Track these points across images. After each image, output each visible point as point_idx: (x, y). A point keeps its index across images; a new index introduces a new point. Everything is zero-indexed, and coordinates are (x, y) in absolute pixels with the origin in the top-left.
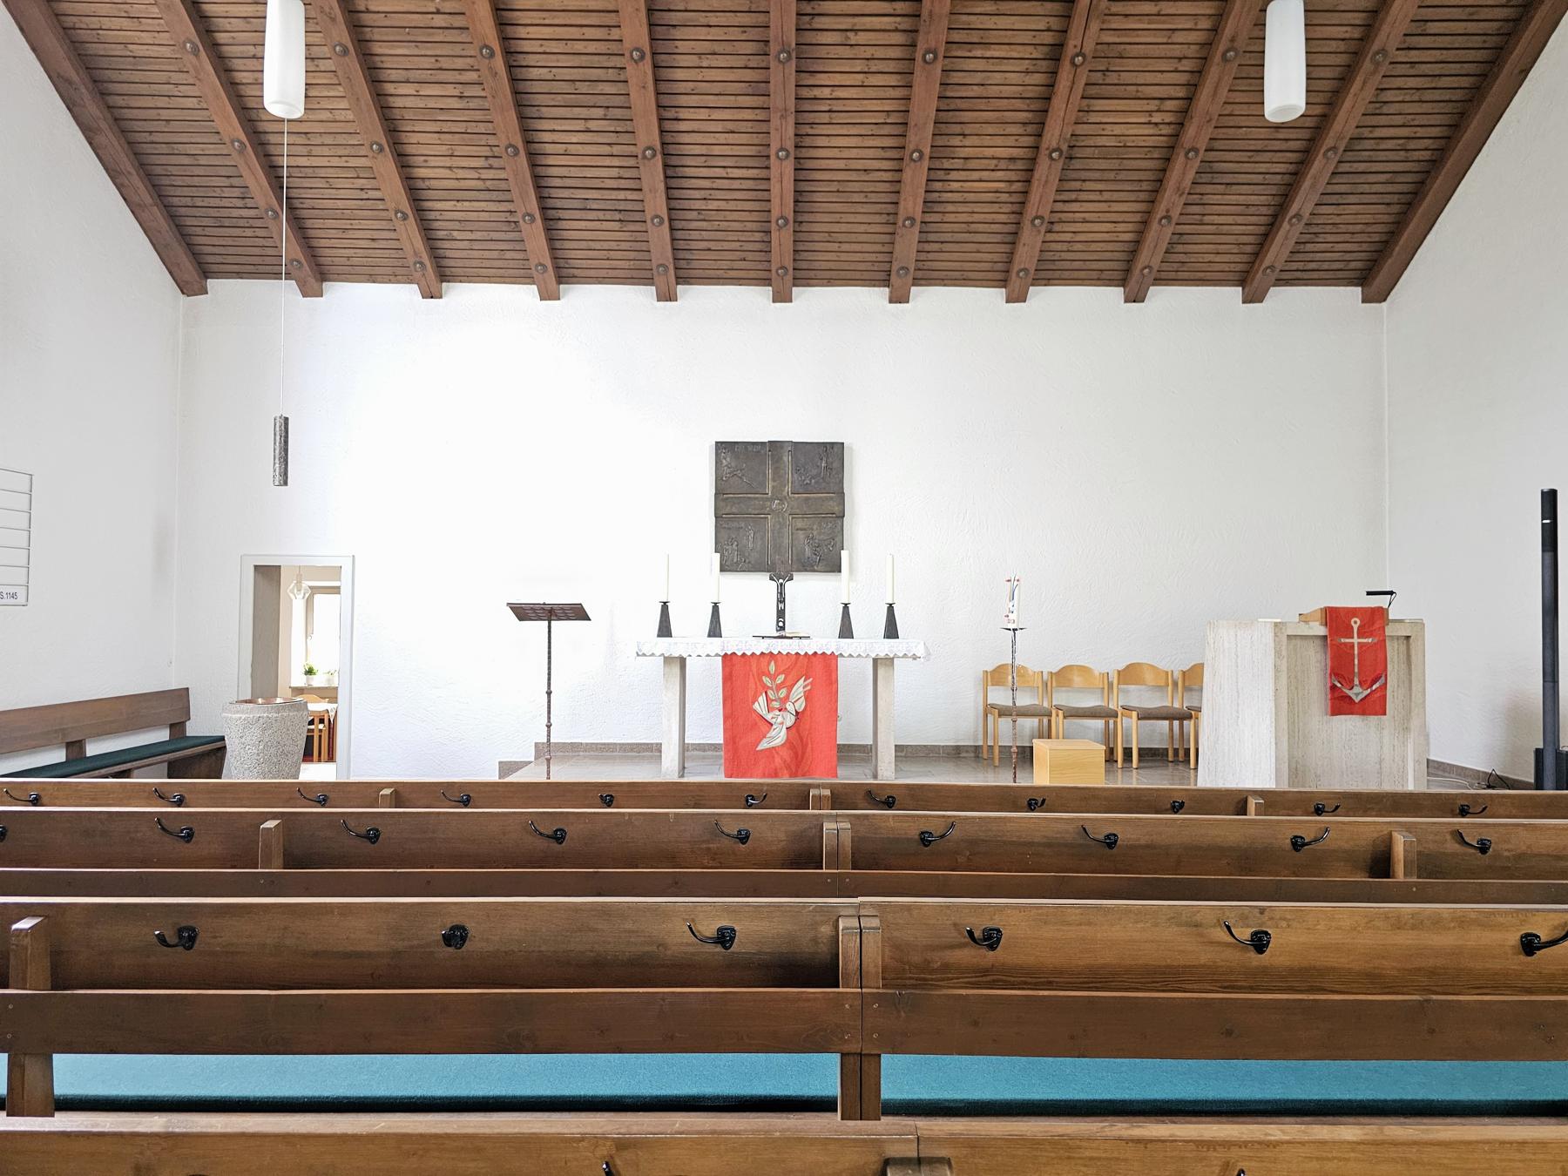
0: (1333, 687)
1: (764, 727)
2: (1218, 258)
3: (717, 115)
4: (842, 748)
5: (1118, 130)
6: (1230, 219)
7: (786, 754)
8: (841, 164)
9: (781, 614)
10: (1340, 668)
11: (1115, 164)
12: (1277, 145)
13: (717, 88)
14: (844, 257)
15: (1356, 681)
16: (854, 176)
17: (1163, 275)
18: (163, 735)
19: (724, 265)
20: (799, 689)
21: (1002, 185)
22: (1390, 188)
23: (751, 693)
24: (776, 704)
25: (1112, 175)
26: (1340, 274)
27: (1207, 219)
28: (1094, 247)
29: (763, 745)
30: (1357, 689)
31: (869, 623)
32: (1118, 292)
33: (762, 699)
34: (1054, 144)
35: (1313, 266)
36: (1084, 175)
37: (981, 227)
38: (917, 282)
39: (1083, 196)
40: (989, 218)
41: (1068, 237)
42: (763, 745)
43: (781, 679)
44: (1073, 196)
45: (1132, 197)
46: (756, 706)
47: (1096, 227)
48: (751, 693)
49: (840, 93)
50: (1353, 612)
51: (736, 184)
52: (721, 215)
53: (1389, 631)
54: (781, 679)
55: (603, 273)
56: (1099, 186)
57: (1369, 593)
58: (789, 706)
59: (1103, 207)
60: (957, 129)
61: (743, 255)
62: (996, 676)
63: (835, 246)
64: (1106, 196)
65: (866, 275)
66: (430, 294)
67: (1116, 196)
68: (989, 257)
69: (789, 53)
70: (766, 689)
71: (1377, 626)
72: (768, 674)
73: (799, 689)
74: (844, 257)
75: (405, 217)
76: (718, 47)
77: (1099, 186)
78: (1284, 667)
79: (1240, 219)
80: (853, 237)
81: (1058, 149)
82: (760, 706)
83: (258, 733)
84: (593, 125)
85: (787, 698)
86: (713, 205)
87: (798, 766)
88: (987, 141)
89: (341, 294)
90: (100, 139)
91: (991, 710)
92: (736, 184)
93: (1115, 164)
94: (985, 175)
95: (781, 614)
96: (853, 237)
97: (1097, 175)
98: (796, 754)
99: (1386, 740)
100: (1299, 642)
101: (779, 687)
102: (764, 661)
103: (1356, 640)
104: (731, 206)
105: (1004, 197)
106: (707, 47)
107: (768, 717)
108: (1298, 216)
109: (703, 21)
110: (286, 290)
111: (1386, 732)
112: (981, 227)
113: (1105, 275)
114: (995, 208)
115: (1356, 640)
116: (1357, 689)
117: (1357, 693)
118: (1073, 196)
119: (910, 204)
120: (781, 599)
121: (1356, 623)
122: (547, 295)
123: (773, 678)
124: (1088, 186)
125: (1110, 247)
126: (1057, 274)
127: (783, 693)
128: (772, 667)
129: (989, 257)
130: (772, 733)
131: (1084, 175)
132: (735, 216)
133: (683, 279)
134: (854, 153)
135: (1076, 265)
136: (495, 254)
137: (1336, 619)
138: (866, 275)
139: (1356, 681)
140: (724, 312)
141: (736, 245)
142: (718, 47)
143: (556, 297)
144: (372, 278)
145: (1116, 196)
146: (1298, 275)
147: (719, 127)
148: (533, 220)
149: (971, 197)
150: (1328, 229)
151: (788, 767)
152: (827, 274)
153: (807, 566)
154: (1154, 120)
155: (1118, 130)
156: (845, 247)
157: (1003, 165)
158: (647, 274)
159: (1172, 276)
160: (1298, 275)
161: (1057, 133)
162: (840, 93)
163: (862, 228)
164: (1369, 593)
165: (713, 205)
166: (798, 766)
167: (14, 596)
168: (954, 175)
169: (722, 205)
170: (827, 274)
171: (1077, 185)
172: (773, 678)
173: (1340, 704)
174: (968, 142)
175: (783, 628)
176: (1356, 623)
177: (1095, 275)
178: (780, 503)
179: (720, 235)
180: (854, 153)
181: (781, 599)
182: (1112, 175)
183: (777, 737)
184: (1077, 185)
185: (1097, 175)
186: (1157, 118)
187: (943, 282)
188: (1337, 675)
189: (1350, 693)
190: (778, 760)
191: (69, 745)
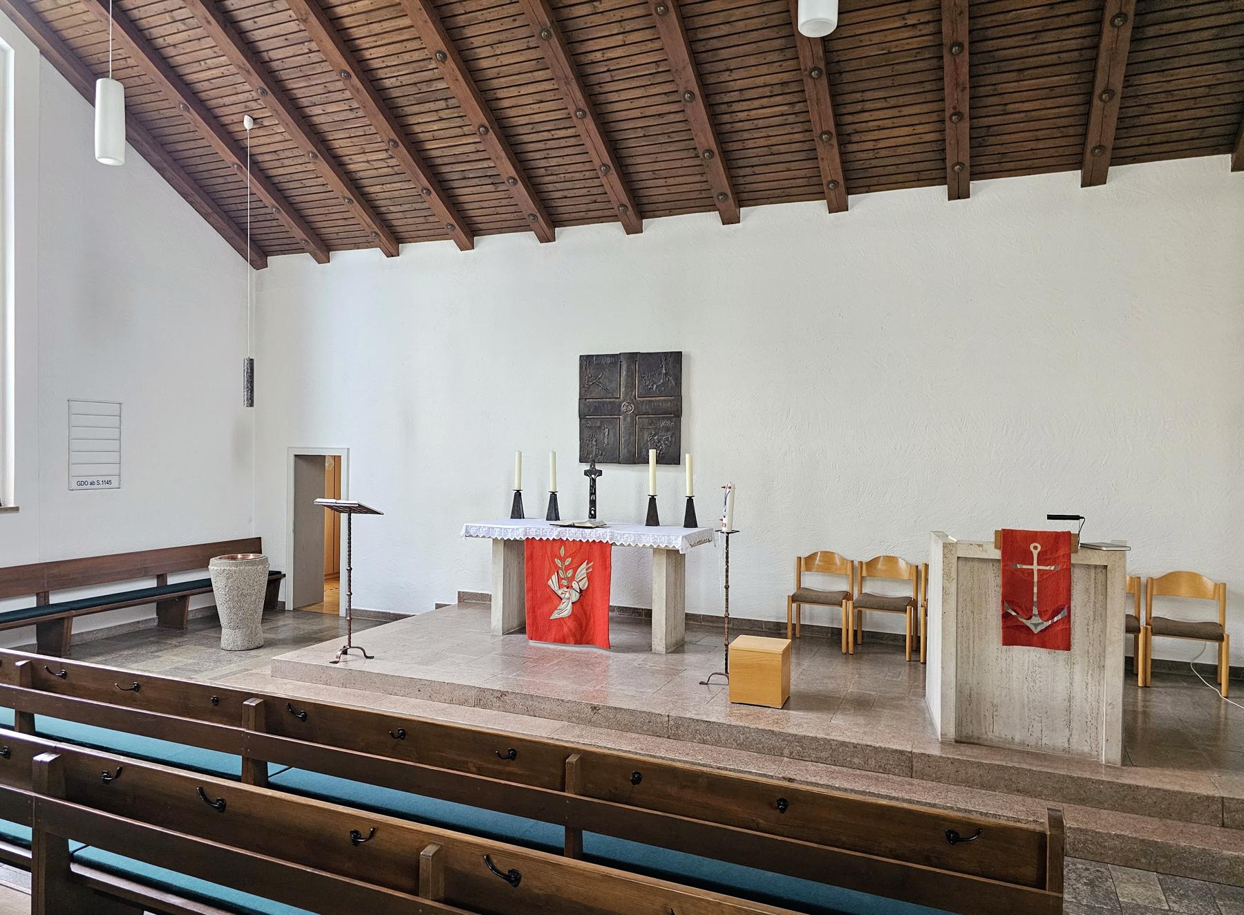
0: (1006, 616)
1: (556, 601)
2: (1041, 145)
3: (524, 90)
4: (689, 617)
5: (876, 38)
6: (1036, 105)
7: (571, 624)
8: (637, 113)
9: (593, 503)
10: (1015, 593)
11: (887, 71)
12: (1058, 22)
13: (516, 68)
14: (673, 189)
15: (1035, 611)
16: (651, 122)
17: (1124, 153)
18: (152, 583)
19: (583, 207)
20: (582, 571)
21: (785, 108)
22: (1221, 44)
23: (546, 572)
24: (565, 582)
25: (889, 82)
26: (1197, 143)
27: (1011, 107)
28: (900, 151)
29: (555, 616)
30: (1036, 620)
31: (672, 511)
32: (942, 190)
33: (554, 577)
34: (810, 65)
35: (1157, 138)
36: (861, 86)
37: (783, 148)
38: (976, 175)
39: (869, 106)
40: (786, 138)
41: (870, 145)
42: (555, 616)
43: (568, 561)
44: (859, 107)
45: (920, 98)
46: (550, 582)
47: (896, 132)
48: (546, 572)
49: (610, 54)
50: (1033, 536)
51: (563, 143)
52: (562, 169)
53: (1075, 559)
54: (568, 561)
55: (499, 225)
56: (881, 94)
57: (1050, 517)
58: (575, 585)
59: (894, 112)
60: (722, 66)
61: (594, 198)
62: (806, 563)
63: (661, 182)
64: (892, 102)
65: (698, 203)
66: (547, 238)
67: (901, 101)
68: (802, 173)
69: (548, 31)
70: (557, 568)
71: (1061, 552)
72: (560, 558)
73: (582, 571)
74: (673, 189)
75: (515, 182)
76: (503, 37)
77: (881, 94)
78: (953, 590)
79: (1049, 103)
80: (673, 172)
81: (814, 69)
82: (553, 583)
83: (224, 581)
84: (443, 114)
85: (572, 578)
86: (553, 162)
87: (582, 635)
88: (754, 71)
89: (341, 258)
90: (168, 174)
91: (801, 597)
92: (563, 143)
93: (887, 71)
94: (765, 101)
95: (593, 503)
96: (673, 172)
97: (874, 84)
98: (580, 625)
99: (1078, 677)
100: (976, 564)
101: (567, 568)
102: (557, 545)
103: (1035, 567)
104: (567, 160)
105: (791, 119)
106: (496, 37)
107: (559, 593)
108: (1107, 90)
109: (482, 18)
110: (304, 261)
111: (1077, 668)
112: (783, 148)
113: (923, 175)
114: (788, 129)
115: (1035, 567)
116: (1036, 620)
117: (1036, 623)
118: (859, 107)
119: (703, 140)
120: (593, 492)
121: (1036, 549)
122: (730, 219)
123: (563, 559)
124: (869, 95)
125: (917, 148)
126: (874, 181)
127: (570, 573)
128: (562, 552)
129: (802, 173)
130: (562, 606)
131: (861, 86)
132: (573, 168)
133: (741, 203)
134: (643, 102)
135: (891, 169)
136: (422, 220)
137: (1013, 543)
138: (698, 203)
139: (1035, 611)
140: (592, 244)
141: (584, 191)
142: (503, 37)
143: (737, 220)
144: (357, 246)
145: (901, 101)
146: (1146, 149)
147: (529, 100)
148: (429, 192)
149: (761, 123)
150: (1162, 97)
151: (574, 635)
152: (667, 205)
153: (615, 459)
154: (910, 22)
155: (876, 38)
156: (671, 181)
157: (777, 90)
158: (708, 202)
159: (996, 167)
160: (1146, 149)
161: (808, 54)
162: (610, 54)
163: (678, 164)
164: (1050, 517)
165: (553, 162)
166: (582, 635)
167: (109, 482)
168: (736, 107)
169: (561, 161)
170: (667, 205)
171: (858, 96)
172: (563, 559)
173: (1014, 634)
174: (735, 75)
175: (593, 516)
176: (1036, 549)
177: (912, 176)
178: (633, 404)
179: (569, 185)
180: (643, 102)
181: (593, 492)
182: (889, 82)
183: (564, 610)
184: (858, 96)
185: (874, 84)
186: (911, 20)
187: (671, 212)
188: (1010, 602)
189: (1028, 623)
190: (566, 630)
191: (158, 577)
